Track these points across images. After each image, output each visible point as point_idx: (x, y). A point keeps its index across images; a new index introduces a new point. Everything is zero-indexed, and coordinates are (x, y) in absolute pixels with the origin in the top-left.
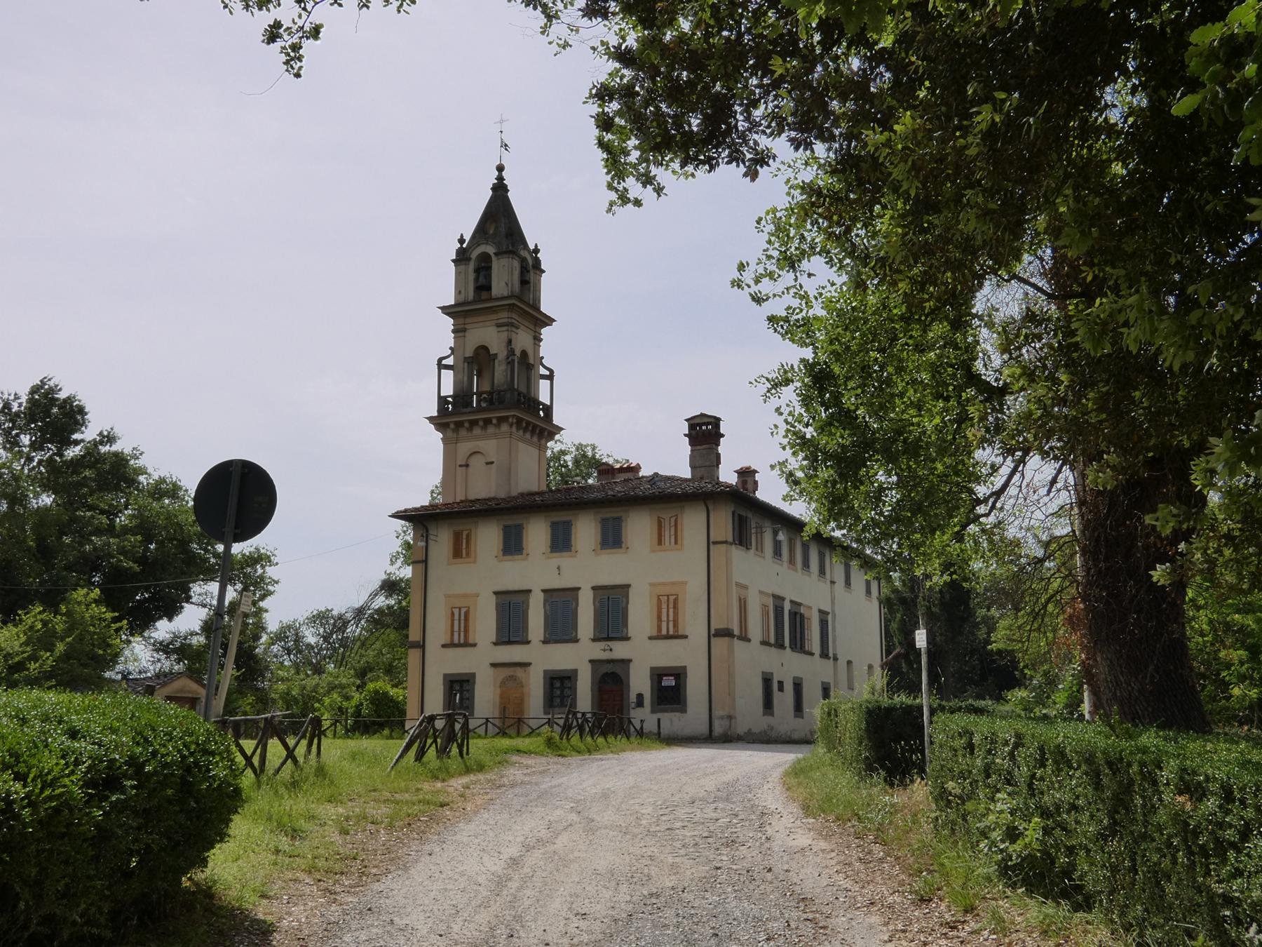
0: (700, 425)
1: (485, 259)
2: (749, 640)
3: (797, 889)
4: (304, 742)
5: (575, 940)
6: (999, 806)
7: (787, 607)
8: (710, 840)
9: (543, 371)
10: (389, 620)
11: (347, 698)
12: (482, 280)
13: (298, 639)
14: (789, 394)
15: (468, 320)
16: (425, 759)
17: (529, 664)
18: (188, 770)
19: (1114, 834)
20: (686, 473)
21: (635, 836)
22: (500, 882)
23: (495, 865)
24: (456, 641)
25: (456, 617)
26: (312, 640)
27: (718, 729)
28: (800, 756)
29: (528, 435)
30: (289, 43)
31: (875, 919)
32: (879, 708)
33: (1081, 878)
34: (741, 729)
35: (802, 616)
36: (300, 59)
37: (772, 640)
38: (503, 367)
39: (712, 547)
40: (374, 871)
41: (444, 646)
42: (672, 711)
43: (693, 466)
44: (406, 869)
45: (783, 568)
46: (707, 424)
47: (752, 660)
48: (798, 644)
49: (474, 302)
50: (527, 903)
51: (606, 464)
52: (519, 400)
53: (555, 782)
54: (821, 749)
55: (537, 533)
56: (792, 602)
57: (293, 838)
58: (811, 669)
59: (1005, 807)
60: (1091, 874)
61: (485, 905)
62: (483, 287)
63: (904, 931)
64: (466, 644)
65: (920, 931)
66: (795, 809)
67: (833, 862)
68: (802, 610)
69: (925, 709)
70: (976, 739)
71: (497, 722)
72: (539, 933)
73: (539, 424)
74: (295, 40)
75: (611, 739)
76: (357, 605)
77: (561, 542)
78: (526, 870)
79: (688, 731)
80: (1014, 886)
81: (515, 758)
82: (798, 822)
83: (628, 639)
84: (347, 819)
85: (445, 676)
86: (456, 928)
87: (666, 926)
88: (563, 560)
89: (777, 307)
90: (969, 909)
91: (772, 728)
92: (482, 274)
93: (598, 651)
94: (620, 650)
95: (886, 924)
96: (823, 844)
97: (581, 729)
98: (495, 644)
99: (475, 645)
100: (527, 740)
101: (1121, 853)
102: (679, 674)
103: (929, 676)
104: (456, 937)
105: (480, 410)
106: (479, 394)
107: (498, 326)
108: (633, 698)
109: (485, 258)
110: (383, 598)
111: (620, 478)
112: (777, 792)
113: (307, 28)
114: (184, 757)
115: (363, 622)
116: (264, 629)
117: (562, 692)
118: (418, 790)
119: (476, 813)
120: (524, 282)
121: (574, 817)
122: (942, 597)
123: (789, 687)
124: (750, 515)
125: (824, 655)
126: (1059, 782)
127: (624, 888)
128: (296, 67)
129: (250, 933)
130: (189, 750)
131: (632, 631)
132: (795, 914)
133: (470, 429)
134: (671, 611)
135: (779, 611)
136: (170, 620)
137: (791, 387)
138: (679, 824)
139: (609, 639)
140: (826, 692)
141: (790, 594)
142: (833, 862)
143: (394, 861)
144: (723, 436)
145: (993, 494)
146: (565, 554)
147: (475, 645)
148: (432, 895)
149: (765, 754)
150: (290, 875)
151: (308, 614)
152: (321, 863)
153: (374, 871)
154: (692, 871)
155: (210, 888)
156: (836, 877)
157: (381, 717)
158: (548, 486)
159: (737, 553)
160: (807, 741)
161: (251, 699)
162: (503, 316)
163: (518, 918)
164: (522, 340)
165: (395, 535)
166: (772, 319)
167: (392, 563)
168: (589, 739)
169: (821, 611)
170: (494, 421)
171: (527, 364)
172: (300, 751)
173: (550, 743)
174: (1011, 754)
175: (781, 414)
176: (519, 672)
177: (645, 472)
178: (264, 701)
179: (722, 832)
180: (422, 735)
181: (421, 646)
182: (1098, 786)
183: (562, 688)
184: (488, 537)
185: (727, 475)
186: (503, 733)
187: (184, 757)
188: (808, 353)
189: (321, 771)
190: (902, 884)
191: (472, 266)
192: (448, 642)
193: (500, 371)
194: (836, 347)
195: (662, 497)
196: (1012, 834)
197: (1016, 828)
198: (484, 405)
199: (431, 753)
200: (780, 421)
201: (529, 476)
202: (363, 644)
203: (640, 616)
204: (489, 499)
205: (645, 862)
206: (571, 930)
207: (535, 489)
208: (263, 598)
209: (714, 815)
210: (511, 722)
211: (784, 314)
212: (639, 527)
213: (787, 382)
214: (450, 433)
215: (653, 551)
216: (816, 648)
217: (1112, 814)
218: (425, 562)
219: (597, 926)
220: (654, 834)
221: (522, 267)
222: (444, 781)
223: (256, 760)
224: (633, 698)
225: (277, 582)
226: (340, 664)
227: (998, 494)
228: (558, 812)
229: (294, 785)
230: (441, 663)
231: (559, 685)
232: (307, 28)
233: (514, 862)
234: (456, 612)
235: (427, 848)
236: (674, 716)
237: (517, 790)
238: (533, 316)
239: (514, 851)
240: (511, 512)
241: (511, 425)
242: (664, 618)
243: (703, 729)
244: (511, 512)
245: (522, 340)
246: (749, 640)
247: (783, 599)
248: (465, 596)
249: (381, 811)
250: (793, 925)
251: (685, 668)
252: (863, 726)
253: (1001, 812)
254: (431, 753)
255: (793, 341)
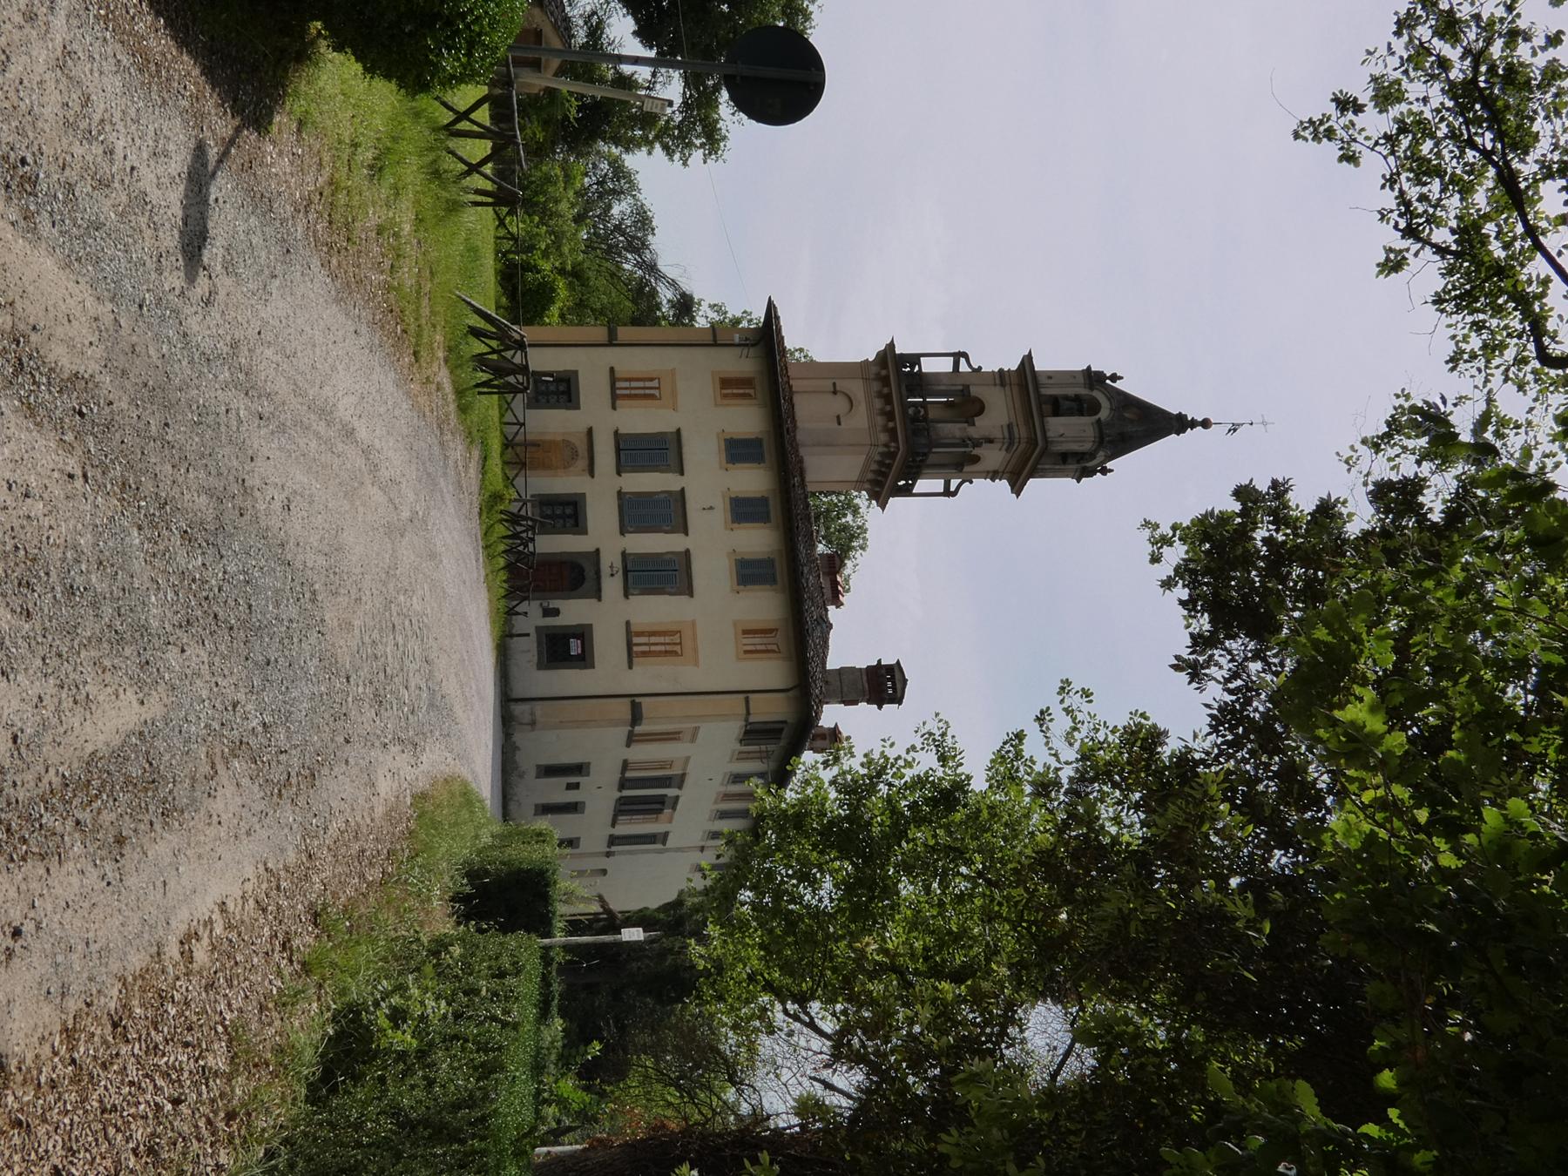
0: (892, 680)
1: (1091, 408)
2: (628, 745)
3: (325, 771)
4: (489, 186)
5: (257, 494)
6: (430, 1003)
7: (671, 792)
8: (381, 675)
9: (954, 483)
10: (644, 305)
11: (546, 255)
12: (1066, 405)
13: (617, 193)
14: (927, 762)
15: (1016, 389)
16: (471, 339)
17: (592, 474)
18: (449, 23)
19: (401, 1125)
20: (833, 662)
21: (385, 584)
22: (325, 412)
23: (345, 408)
24: (618, 384)
25: (648, 384)
26: (615, 210)
27: (518, 709)
28: (488, 802)
29: (874, 467)
30: (1336, 127)
31: (291, 857)
32: (547, 885)
33: (347, 1092)
34: (518, 738)
35: (660, 811)
36: (1316, 138)
37: (629, 774)
38: (958, 434)
39: (742, 696)
40: (334, 261)
41: (612, 370)
42: (540, 653)
43: (841, 672)
44: (338, 301)
45: (718, 786)
46: (894, 688)
47: (605, 750)
48: (625, 807)
49: (1039, 395)
50: (302, 442)
51: (843, 565)
52: (918, 454)
53: (448, 497)
54: (497, 828)
55: (753, 480)
56: (677, 798)
57: (371, 167)
58: (594, 825)
59: (430, 1011)
60: (356, 1101)
61: (297, 391)
62: (1057, 406)
63: (278, 888)
64: (614, 397)
65: (279, 907)
66: (423, 785)
67: (359, 818)
68: (667, 811)
69: (547, 941)
70: (510, 981)
71: (520, 438)
72: (265, 452)
73: (888, 480)
74: (1340, 133)
75: (503, 576)
76: (661, 266)
77: (743, 510)
78: (340, 447)
79: (515, 672)
80: (334, 1020)
81: (476, 454)
82: (405, 785)
83: (626, 595)
84: (396, 235)
85: (576, 372)
86: (269, 352)
87: (277, 605)
88: (721, 514)
89: (1033, 747)
90: (306, 969)
91: (521, 776)
92: (1074, 405)
93: (610, 560)
94: (612, 586)
95: (286, 869)
96: (380, 811)
97: (515, 536)
98: (616, 433)
99: (614, 408)
100: (498, 470)
101: (377, 1133)
102: (585, 660)
103: (587, 945)
104: (258, 351)
105: (905, 406)
106: (924, 405)
107: (1010, 426)
108: (554, 604)
109: (1094, 408)
110: (669, 295)
111: (824, 582)
112: (443, 767)
113: (1354, 147)
114: (463, 16)
115: (640, 272)
116: (627, 150)
117: (559, 517)
118: (434, 326)
119: (408, 393)
120: (1065, 457)
121: (406, 514)
122: (685, 969)
123: (572, 796)
124: (783, 743)
125: (613, 840)
126: (461, 1067)
127: (321, 561)
128: (1306, 134)
129: (257, 105)
130: (472, 22)
131: (636, 600)
132: (295, 762)
133: (880, 395)
134: (662, 648)
135: (665, 782)
136: (635, 33)
137: (936, 764)
138: (400, 640)
139: (626, 572)
140: (571, 843)
141: (686, 795)
142: (359, 818)
143: (348, 287)
144: (880, 708)
145: (812, 1018)
146: (724, 455)
147: (614, 408)
148: (308, 329)
149: (489, 764)
150: (326, 158)
151: (648, 205)
152: (342, 198)
153: (334, 261)
154: (344, 647)
155: (310, 59)
156: (341, 820)
157: (523, 294)
158: (813, 494)
159: (735, 728)
160: (506, 815)
161: (540, 136)
162: (1022, 432)
163: (282, 429)
164: (993, 456)
165: (748, 307)
166: (1020, 736)
167: (712, 307)
168: (502, 547)
169: (666, 834)
170: (891, 425)
171: (962, 463)
172: (477, 181)
173: (496, 498)
174: (494, 1018)
175: (908, 752)
176: (582, 463)
177: (833, 612)
178: (538, 152)
179: (392, 692)
180: (502, 335)
181: (612, 342)
182: (456, 1107)
183: (564, 517)
184: (747, 420)
185: (831, 715)
186: (508, 444)
187: (463, 16)
188: (979, 784)
189: (454, 207)
190: (335, 895)
191: (1083, 391)
192: (617, 375)
193: (954, 430)
194: (985, 814)
195: (802, 633)
196: (398, 1017)
197: (405, 1021)
198: (911, 411)
199: (479, 347)
200: (899, 750)
201: (826, 469)
202: (613, 275)
203: (654, 610)
204: (794, 421)
205: (354, 591)
206: (270, 491)
207: (809, 477)
208: (666, 148)
209: (412, 685)
210: (521, 454)
211: (1026, 755)
212: (764, 605)
213: (943, 759)
214: (874, 369)
215: (735, 624)
216: (623, 829)
217: (425, 1122)
218: (715, 344)
219: (275, 522)
220: (387, 608)
221: (1083, 454)
222: (446, 361)
223: (464, 125)
224: (554, 604)
225: (685, 164)
226: (590, 246)
227: (812, 1025)
228: (411, 496)
229: (436, 174)
230: (591, 367)
231: (569, 513)
232: (1354, 147)
233: (349, 433)
234: (655, 384)
235: (364, 329)
236: (533, 656)
237: (436, 449)
238: (1023, 468)
239: (362, 434)
240: (779, 447)
241: (886, 445)
242: (653, 639)
243: (519, 690)
244: (779, 447)
245: (993, 456)
246: (628, 745)
247: (680, 788)
248: (674, 394)
249: (407, 276)
250: (283, 757)
251: (593, 667)
252: (525, 866)
253: (422, 1003)
254: (479, 347)
255: (992, 761)
